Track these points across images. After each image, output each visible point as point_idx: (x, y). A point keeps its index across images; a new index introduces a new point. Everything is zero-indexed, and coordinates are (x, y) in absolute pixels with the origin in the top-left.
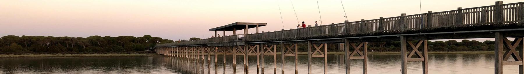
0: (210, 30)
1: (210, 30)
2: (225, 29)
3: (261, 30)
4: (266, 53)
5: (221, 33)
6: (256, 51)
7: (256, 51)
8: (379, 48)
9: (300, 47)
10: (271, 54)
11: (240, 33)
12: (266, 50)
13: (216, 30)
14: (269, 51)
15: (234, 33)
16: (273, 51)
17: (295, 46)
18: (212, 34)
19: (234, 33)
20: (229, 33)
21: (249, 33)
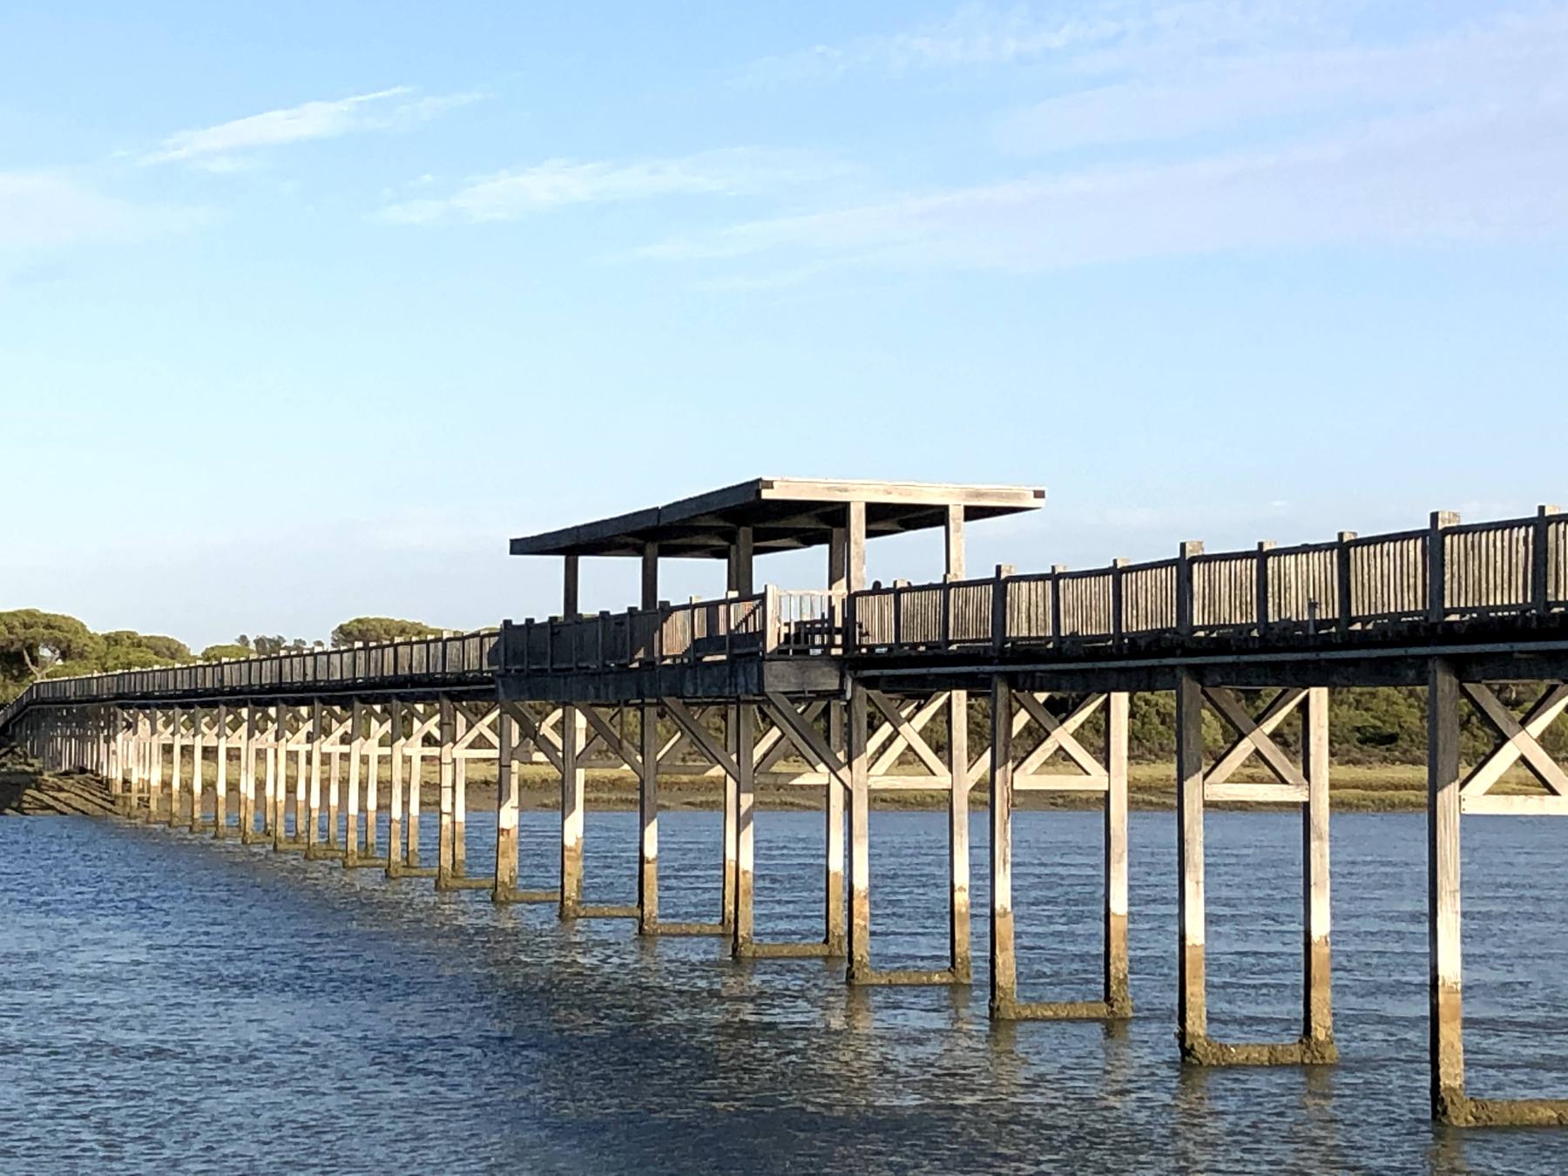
0: (521, 547)
1: (521, 547)
2: (651, 535)
3: (974, 552)
4: (1030, 776)
5: (610, 585)
6: (943, 748)
7: (943, 748)
8: (1262, 705)
9: (1349, 715)
10: (1094, 779)
11: (793, 584)
12: (1036, 735)
13: (574, 544)
14: (1062, 754)
15: (740, 579)
16: (471, 746)
17: (1304, 706)
18: (535, 594)
19: (740, 579)
20: (692, 579)
21: (717, 569)
